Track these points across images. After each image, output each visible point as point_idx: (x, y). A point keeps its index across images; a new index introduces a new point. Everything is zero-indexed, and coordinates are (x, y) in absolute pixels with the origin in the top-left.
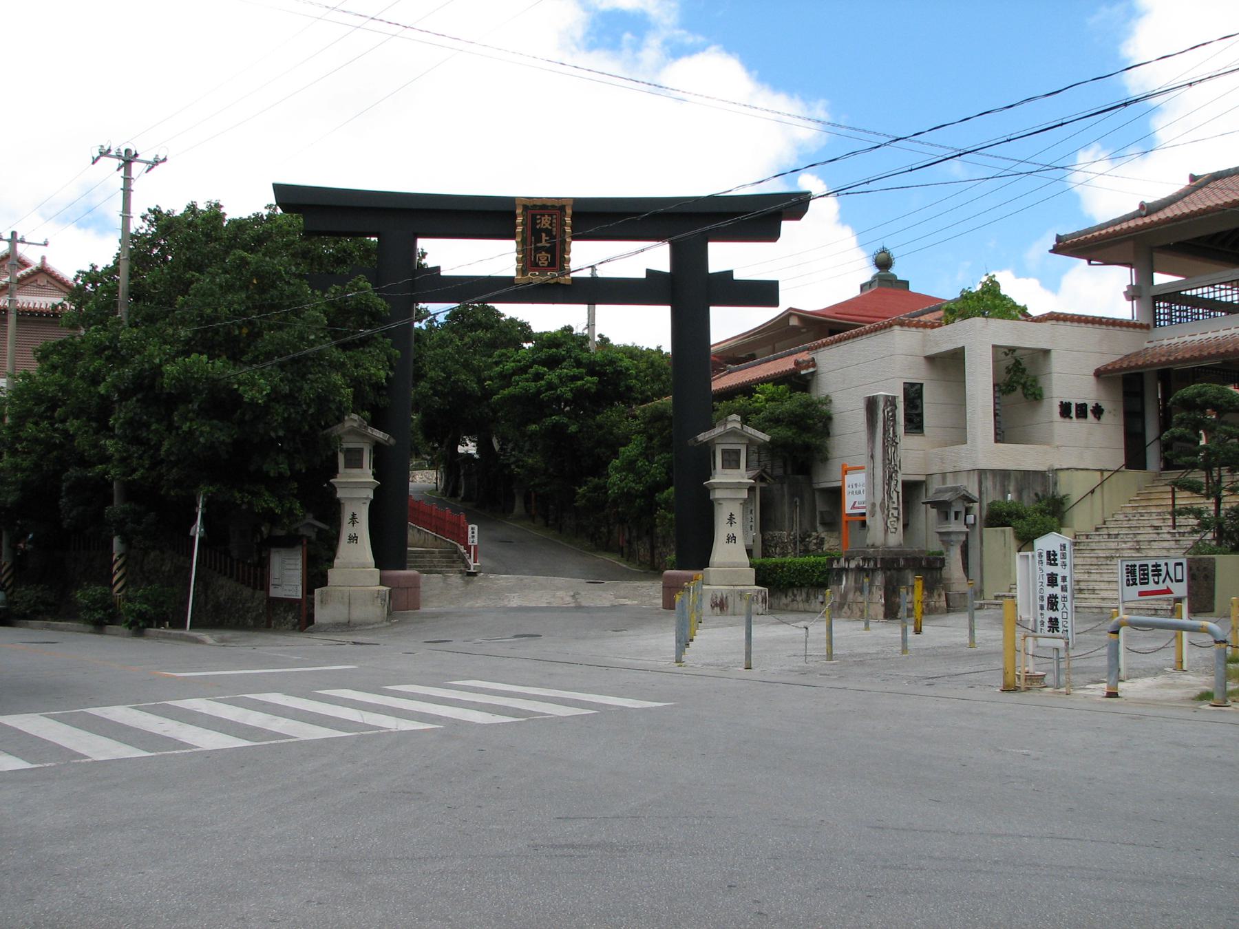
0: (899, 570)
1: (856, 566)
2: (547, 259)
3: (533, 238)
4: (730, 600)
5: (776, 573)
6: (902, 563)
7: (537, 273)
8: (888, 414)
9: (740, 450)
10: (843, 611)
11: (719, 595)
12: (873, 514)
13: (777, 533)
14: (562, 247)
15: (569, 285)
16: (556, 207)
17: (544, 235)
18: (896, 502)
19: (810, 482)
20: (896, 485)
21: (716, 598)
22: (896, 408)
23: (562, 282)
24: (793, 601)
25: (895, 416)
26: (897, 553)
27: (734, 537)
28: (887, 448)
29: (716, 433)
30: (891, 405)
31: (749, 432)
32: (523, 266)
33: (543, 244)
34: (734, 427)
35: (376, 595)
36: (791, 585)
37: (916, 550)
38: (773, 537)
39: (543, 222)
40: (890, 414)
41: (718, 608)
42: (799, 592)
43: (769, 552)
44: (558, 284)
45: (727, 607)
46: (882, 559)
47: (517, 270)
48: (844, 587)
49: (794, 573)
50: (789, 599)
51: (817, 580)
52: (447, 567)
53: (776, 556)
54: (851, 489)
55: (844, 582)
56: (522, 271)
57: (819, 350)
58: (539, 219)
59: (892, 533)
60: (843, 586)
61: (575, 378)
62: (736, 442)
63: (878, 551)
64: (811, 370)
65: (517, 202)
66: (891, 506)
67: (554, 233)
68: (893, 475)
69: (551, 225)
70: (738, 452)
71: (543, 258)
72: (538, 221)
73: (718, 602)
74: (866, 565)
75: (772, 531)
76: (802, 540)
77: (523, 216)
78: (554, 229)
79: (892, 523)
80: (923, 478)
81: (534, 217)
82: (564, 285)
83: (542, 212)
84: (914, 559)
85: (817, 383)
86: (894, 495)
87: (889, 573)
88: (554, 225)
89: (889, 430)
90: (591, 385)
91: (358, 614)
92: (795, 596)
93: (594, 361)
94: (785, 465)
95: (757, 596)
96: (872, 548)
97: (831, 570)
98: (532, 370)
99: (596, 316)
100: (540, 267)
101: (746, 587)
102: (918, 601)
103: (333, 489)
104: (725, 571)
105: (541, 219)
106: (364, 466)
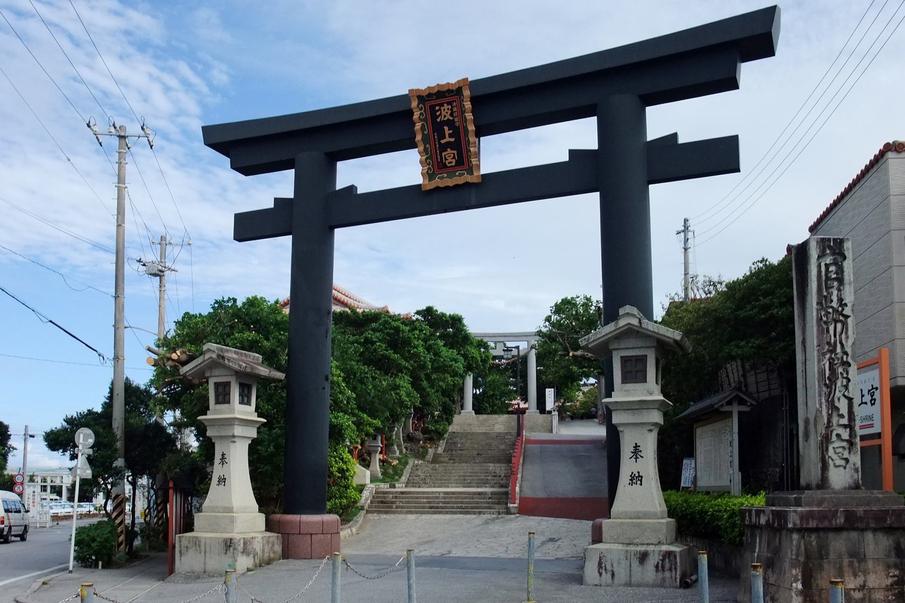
2: (454, 157)
3: (436, 134)
14: (467, 139)
15: (479, 183)
16: (453, 91)
17: (446, 128)
18: (846, 415)
27: (639, 476)
32: (429, 169)
33: (448, 139)
34: (629, 324)
39: (444, 113)
44: (467, 184)
47: (423, 174)
48: (758, 555)
56: (429, 175)
58: (438, 111)
59: (836, 466)
65: (410, 95)
66: (835, 420)
67: (457, 124)
69: (451, 115)
71: (450, 156)
72: (438, 113)
77: (421, 109)
78: (456, 120)
79: (838, 450)
81: (432, 108)
82: (474, 184)
83: (439, 101)
88: (455, 114)
99: (240, 137)
104: (623, 524)
105: (440, 110)
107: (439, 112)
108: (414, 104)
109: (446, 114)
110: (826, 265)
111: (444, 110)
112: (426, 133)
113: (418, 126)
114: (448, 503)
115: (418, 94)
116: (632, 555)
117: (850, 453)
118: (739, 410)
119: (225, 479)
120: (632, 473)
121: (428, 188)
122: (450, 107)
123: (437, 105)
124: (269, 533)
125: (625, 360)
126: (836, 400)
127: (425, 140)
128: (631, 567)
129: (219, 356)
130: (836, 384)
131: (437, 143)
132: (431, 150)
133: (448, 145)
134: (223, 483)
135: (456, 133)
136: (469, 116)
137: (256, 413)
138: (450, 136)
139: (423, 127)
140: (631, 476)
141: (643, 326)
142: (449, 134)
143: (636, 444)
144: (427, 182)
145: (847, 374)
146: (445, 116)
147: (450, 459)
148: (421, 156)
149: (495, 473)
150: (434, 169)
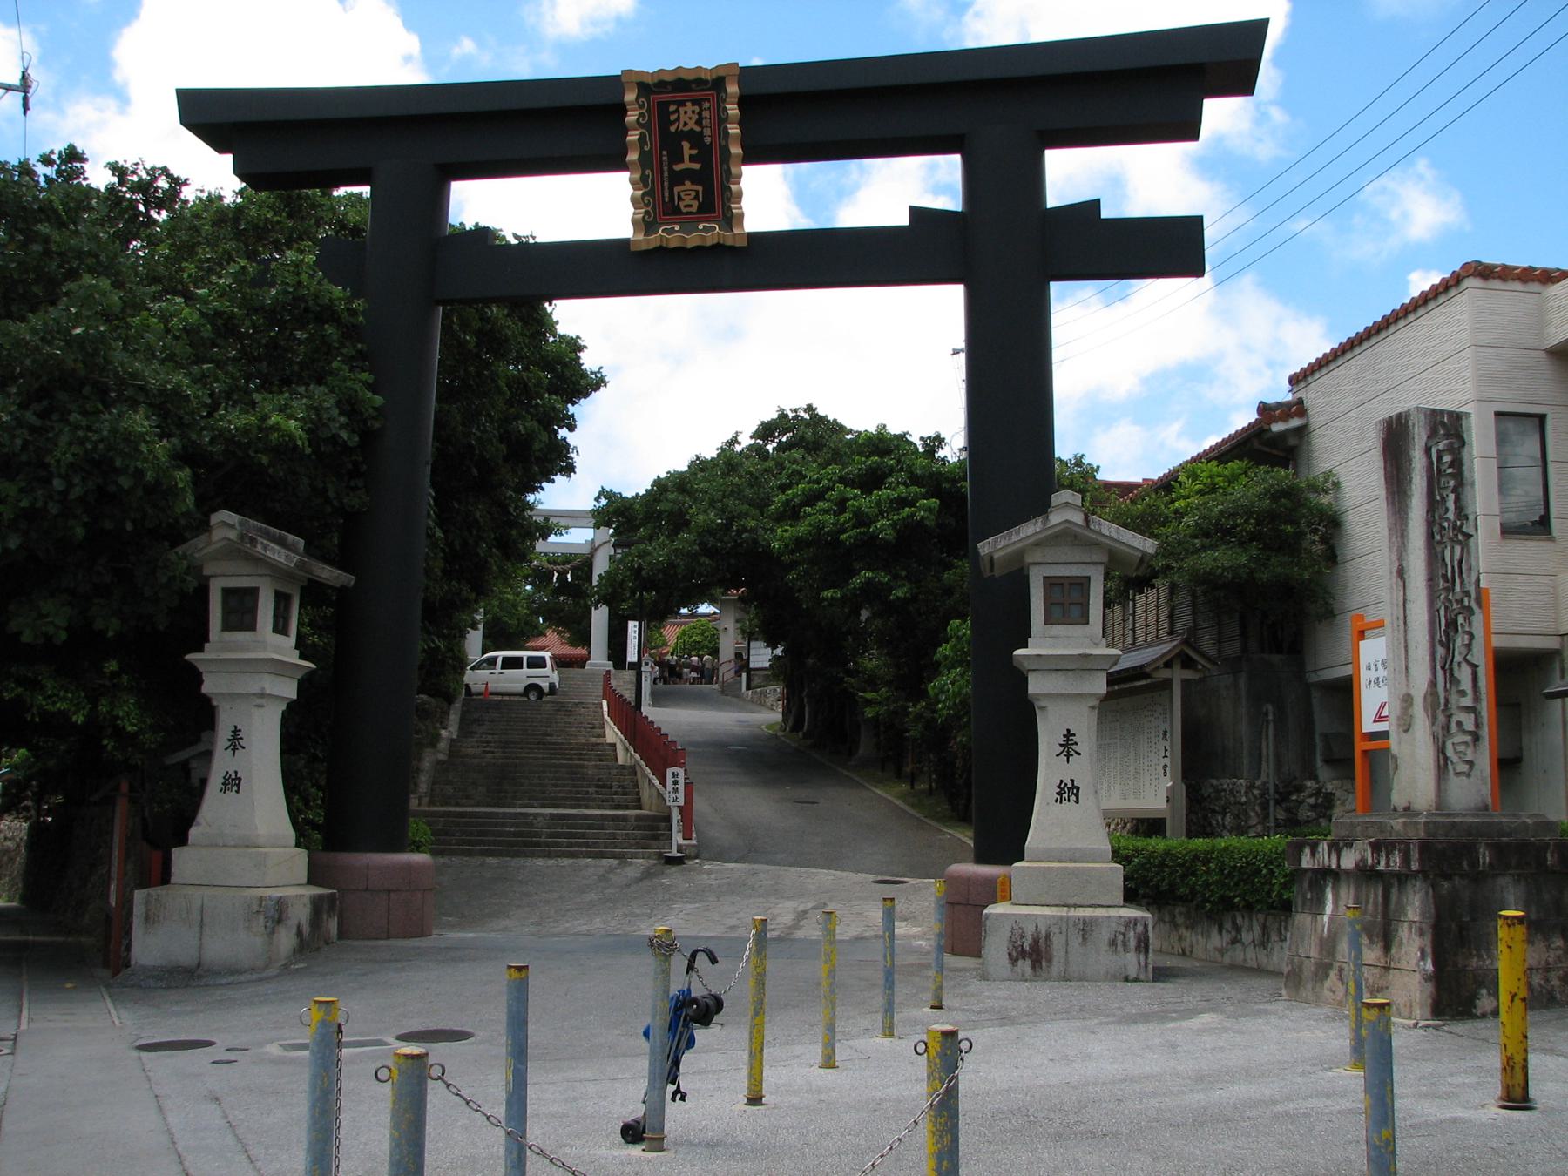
0: (1478, 878)
1: (1357, 865)
2: (696, 198)
3: (665, 153)
4: (1057, 942)
5: (1194, 874)
6: (1485, 857)
7: (677, 228)
8: (1440, 458)
9: (1088, 578)
10: (1328, 983)
11: (1030, 929)
12: (1406, 726)
13: (1226, 783)
14: (725, 167)
17: (686, 145)
18: (1469, 690)
19: (1300, 672)
20: (1469, 646)
21: (1023, 936)
22: (1463, 443)
23: (729, 243)
24: (1234, 941)
25: (1461, 465)
26: (1472, 831)
27: (1074, 787)
28: (1439, 549)
29: (1022, 536)
30: (1447, 436)
31: (1105, 532)
32: (647, 213)
33: (687, 164)
34: (1067, 521)
35: (255, 908)
36: (1227, 905)
37: (1529, 821)
38: (1218, 791)
39: (683, 118)
40: (1447, 458)
41: (1028, 962)
42: (1247, 922)
43: (1210, 824)
44: (719, 248)
45: (1049, 961)
46: (1424, 848)
47: (634, 222)
48: (1331, 920)
49: (1230, 875)
50: (1227, 938)
51: (1280, 895)
52: (638, 846)
53: (1225, 832)
54: (1372, 675)
55: (1329, 908)
56: (645, 224)
57: (1310, 379)
60: (1326, 918)
61: (902, 502)
62: (1077, 559)
63: (1416, 823)
64: (1295, 422)
65: (623, 80)
66: (1454, 698)
67: (707, 141)
68: (1461, 620)
69: (699, 122)
70: (1083, 584)
71: (689, 194)
72: (673, 118)
73: (1026, 946)
74: (1383, 862)
75: (1217, 778)
76: (1282, 799)
77: (641, 107)
78: (707, 132)
80: (1551, 643)
81: (663, 108)
82: (732, 249)
83: (680, 96)
84: (1523, 848)
85: (1309, 451)
86: (1464, 675)
87: (1446, 885)
89: (1444, 499)
90: (927, 514)
91: (221, 947)
92: (1238, 930)
93: (940, 473)
94: (1244, 634)
95: (1124, 935)
96: (1402, 816)
97: (1298, 874)
98: (834, 495)
100: (682, 213)
101: (1099, 912)
102: (1513, 996)
103: (196, 677)
105: (677, 111)
106: (259, 625)
107: (675, 116)
108: (630, 97)
109: (688, 120)
110: (1439, 452)
111: (686, 112)
112: (646, 148)
113: (633, 136)
114: (558, 835)
115: (638, 80)
116: (1071, 926)
117: (1475, 752)
118: (1183, 677)
119: (240, 779)
120: (1062, 781)
121: (644, 247)
122: (697, 109)
123: (674, 103)
124: (311, 887)
125: (1050, 583)
126: (1455, 666)
127: (644, 160)
128: (1067, 945)
129: (242, 537)
130: (1454, 641)
131: (666, 168)
132: (653, 179)
133: (688, 175)
134: (235, 788)
135: (704, 154)
136: (734, 130)
137: (297, 652)
138: (692, 159)
139: (642, 139)
140: (1059, 787)
141: (1092, 527)
142: (691, 156)
143: (1068, 731)
144: (641, 237)
145: (1470, 624)
146: (685, 124)
147: (485, 752)
148: (635, 189)
149: (599, 780)
150: (655, 214)
